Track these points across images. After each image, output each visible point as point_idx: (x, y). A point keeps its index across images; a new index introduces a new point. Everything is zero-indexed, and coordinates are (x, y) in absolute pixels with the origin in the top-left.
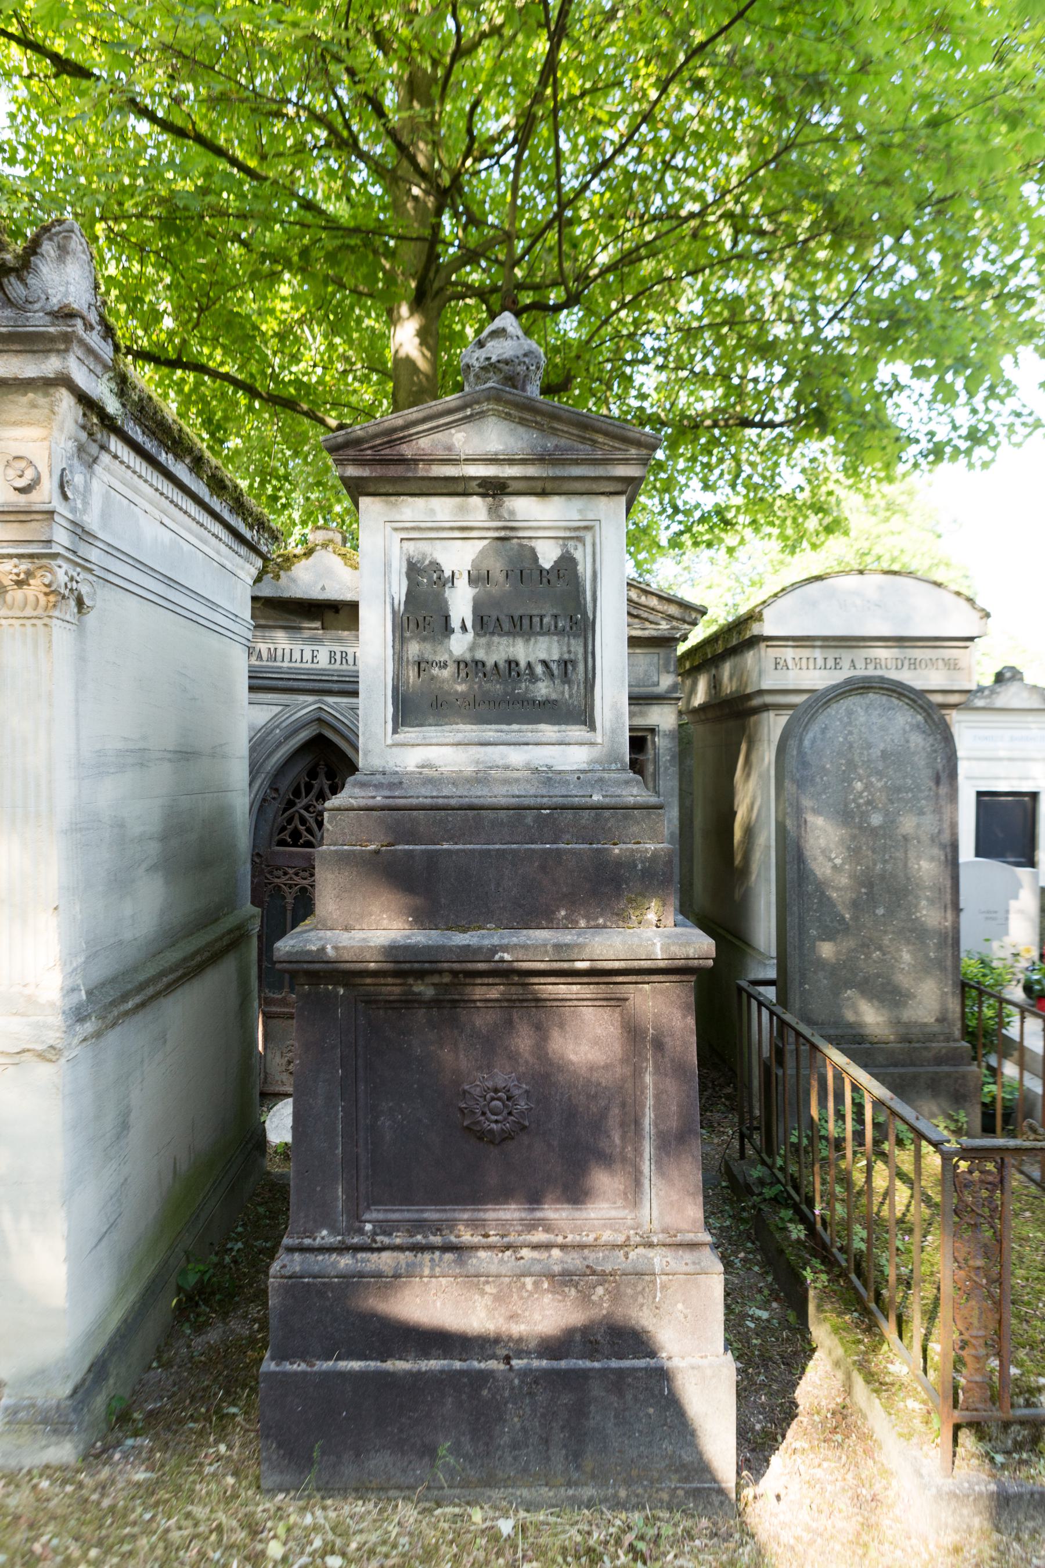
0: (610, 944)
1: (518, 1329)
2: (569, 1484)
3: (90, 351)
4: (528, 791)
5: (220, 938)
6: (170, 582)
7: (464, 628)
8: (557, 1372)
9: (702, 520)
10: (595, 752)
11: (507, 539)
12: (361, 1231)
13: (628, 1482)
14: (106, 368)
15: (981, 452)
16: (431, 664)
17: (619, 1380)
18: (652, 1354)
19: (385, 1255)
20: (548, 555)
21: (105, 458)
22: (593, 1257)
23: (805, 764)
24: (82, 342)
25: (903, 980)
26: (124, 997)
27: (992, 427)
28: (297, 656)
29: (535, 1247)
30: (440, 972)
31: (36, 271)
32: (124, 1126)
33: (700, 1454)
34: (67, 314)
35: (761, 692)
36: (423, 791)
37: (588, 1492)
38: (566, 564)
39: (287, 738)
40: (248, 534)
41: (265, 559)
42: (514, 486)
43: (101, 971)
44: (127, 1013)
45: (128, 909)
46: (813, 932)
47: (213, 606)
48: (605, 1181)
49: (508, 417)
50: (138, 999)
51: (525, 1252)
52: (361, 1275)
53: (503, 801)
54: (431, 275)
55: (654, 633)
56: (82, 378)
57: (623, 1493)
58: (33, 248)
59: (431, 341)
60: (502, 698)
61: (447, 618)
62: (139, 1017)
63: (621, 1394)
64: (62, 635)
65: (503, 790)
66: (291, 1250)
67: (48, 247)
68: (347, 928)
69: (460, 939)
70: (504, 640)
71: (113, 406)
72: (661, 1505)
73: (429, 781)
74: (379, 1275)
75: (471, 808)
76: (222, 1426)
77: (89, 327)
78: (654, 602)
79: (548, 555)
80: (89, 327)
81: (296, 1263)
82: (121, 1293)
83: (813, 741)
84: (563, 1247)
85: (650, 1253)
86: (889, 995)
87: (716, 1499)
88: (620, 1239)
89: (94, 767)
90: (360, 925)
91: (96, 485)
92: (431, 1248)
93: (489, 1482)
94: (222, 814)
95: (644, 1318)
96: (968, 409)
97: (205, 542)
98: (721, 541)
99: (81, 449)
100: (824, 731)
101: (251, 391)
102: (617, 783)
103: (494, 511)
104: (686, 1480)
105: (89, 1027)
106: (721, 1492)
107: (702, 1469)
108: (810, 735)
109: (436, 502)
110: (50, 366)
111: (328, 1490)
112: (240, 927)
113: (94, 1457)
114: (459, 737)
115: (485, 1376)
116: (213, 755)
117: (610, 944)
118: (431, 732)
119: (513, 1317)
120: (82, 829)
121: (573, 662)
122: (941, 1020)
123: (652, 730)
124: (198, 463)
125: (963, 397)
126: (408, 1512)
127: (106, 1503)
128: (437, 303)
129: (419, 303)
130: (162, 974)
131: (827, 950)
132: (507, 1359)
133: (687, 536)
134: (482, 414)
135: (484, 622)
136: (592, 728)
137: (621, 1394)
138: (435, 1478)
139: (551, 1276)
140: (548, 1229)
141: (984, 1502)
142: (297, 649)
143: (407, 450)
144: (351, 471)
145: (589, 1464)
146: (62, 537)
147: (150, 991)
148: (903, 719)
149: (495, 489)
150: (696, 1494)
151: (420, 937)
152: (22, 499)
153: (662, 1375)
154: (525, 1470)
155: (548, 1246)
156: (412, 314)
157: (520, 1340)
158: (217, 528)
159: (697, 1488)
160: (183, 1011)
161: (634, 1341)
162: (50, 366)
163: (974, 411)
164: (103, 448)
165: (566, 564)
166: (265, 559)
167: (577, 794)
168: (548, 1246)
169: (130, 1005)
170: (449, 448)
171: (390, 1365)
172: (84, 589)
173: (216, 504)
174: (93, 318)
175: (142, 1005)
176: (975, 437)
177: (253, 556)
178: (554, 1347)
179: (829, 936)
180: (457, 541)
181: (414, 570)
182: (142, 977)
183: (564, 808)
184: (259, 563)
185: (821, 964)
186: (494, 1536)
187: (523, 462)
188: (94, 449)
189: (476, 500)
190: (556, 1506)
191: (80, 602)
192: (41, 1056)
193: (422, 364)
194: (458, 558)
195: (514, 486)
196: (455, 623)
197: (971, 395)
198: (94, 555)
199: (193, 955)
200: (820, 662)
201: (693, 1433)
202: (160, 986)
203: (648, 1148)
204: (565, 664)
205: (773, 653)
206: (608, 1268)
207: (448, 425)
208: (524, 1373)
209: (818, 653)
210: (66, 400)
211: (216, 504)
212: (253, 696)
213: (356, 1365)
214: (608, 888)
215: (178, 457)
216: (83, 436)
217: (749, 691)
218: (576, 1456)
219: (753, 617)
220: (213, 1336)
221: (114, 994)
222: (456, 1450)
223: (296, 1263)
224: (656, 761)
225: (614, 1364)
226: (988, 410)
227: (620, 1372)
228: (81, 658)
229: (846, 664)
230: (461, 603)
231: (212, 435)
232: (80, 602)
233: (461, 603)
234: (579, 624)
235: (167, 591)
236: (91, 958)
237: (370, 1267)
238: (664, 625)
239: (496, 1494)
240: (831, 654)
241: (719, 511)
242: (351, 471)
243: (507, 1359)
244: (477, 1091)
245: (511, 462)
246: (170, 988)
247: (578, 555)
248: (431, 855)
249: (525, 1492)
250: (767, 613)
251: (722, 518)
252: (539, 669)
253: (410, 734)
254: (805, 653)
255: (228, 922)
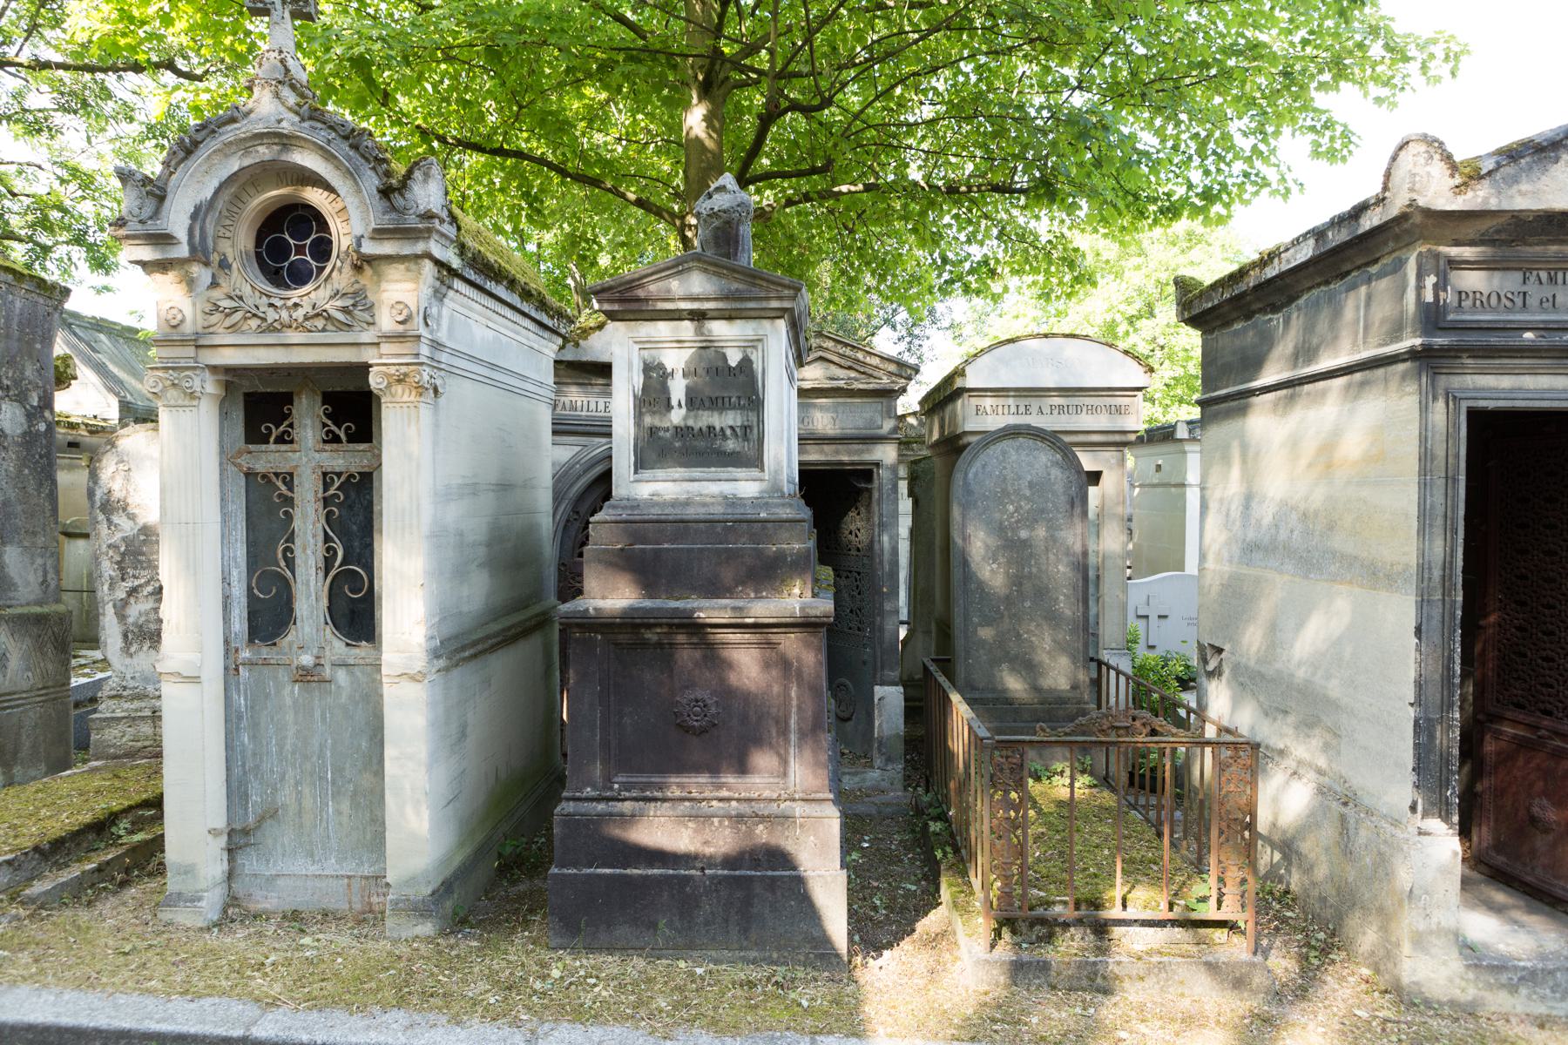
0: (763, 609)
1: (709, 850)
2: (741, 949)
3: (443, 235)
4: (718, 510)
5: (530, 619)
6: (493, 366)
7: (680, 405)
8: (734, 877)
9: (972, 271)
10: (764, 485)
11: (707, 347)
12: (611, 789)
13: (778, 949)
14: (452, 242)
15: (1217, 208)
16: (658, 429)
17: (772, 883)
18: (795, 868)
19: (627, 804)
20: (734, 358)
21: (451, 293)
22: (756, 806)
23: (969, 492)
24: (438, 232)
25: (1042, 657)
26: (463, 648)
27: (1224, 186)
28: (592, 406)
29: (721, 800)
30: (660, 625)
31: (411, 189)
32: (463, 734)
33: (824, 931)
34: (429, 216)
35: (965, 433)
36: (653, 511)
37: (753, 954)
38: (746, 363)
39: (585, 472)
40: (549, 323)
41: (564, 338)
42: (710, 314)
43: (449, 629)
44: (465, 659)
45: (465, 591)
46: (976, 620)
47: (524, 378)
48: (763, 760)
49: (706, 271)
50: (472, 651)
51: (714, 803)
52: (611, 815)
53: (702, 517)
54: (717, 67)
55: (871, 386)
56: (437, 252)
57: (775, 955)
58: (409, 175)
59: (717, 124)
60: (696, 449)
61: (669, 399)
62: (472, 664)
63: (774, 892)
64: (425, 412)
65: (702, 510)
66: (568, 799)
67: (417, 174)
68: (603, 598)
69: (673, 604)
70: (706, 413)
71: (456, 263)
72: (799, 963)
73: (656, 504)
74: (622, 815)
75: (682, 521)
76: (526, 924)
77: (442, 221)
78: (875, 361)
79: (734, 358)
80: (442, 221)
81: (570, 807)
82: (461, 845)
83: (976, 474)
84: (738, 800)
85: (794, 804)
86: (1028, 667)
87: (834, 961)
88: (775, 796)
89: (444, 496)
90: (610, 596)
91: (445, 311)
92: (655, 800)
93: (691, 946)
94: (532, 529)
95: (789, 846)
96: (1200, 171)
97: (518, 333)
98: (988, 288)
99: (436, 291)
100: (984, 466)
101: (563, 172)
102: (777, 505)
103: (699, 331)
104: (815, 948)
105: (442, 663)
106: (838, 956)
107: (825, 941)
108: (973, 470)
109: (661, 325)
110: (420, 247)
111: (590, 949)
112: (544, 613)
113: (443, 933)
114: (677, 476)
115: (688, 878)
116: (525, 486)
117: (763, 609)
118: (660, 473)
119: (706, 843)
120: (437, 536)
121: (751, 427)
122: (1074, 687)
123: (877, 464)
124: (512, 283)
125: (1196, 161)
126: (639, 962)
127: (453, 953)
128: (721, 91)
129: (706, 90)
130: (488, 637)
131: (986, 633)
132: (703, 869)
133: (958, 284)
134: (689, 269)
135: (694, 401)
136: (763, 470)
137: (774, 892)
138: (656, 942)
139: (730, 817)
140: (729, 790)
141: (1006, 967)
142: (593, 401)
143: (641, 293)
144: (606, 307)
145: (753, 936)
146: (425, 350)
147: (480, 647)
148: (1043, 460)
149: (699, 316)
150: (822, 957)
151: (648, 603)
152: (401, 328)
153: (800, 881)
154: (713, 939)
155: (729, 800)
156: (700, 101)
157: (711, 857)
158: (527, 323)
159: (820, 952)
160: (502, 664)
161: (779, 858)
162: (420, 247)
163: (1207, 173)
164: (450, 287)
165: (746, 363)
166: (564, 338)
167: (750, 513)
168: (729, 800)
169: (467, 654)
170: (669, 291)
171: (628, 871)
172: (439, 382)
173: (525, 307)
174: (444, 214)
175: (474, 656)
176: (1208, 196)
177: (555, 337)
178: (730, 862)
179: (987, 622)
180: (674, 347)
181: (648, 368)
182: (475, 637)
183: (741, 521)
184: (560, 341)
185: (983, 643)
186: (692, 974)
187: (715, 299)
188: (444, 289)
189: (687, 323)
190: (732, 962)
191: (436, 391)
192: (413, 678)
193: (709, 144)
194: (675, 360)
195: (710, 314)
196: (674, 402)
197: (1203, 158)
198: (444, 357)
199: (509, 628)
200: (1013, 409)
201: (819, 918)
202: (486, 646)
203: (793, 737)
204: (745, 428)
205: (974, 401)
206: (766, 813)
207: (668, 277)
208: (713, 877)
209: (1011, 401)
210: (428, 266)
211: (525, 307)
212: (558, 438)
213: (608, 871)
214: (767, 573)
215: (498, 282)
216: (438, 284)
217: (959, 431)
218: (745, 931)
219: (959, 372)
220: (522, 888)
221: (456, 645)
222: (670, 925)
223: (570, 807)
224: (880, 490)
225: (770, 873)
226: (1218, 170)
227: (773, 878)
228: (436, 425)
229: (1034, 409)
230: (678, 389)
231: (531, 205)
232: (436, 391)
233: (678, 389)
234: (752, 400)
235: (492, 373)
236: (443, 620)
237: (615, 810)
238: (885, 380)
239: (695, 954)
240: (1023, 402)
241: (985, 262)
242: (606, 307)
243: (703, 869)
244: (684, 701)
245: (708, 299)
246: (493, 649)
247: (753, 358)
248: (657, 553)
249: (713, 953)
250: (968, 369)
251: (987, 269)
252: (728, 432)
253: (647, 474)
254: (1001, 401)
255: (537, 609)
